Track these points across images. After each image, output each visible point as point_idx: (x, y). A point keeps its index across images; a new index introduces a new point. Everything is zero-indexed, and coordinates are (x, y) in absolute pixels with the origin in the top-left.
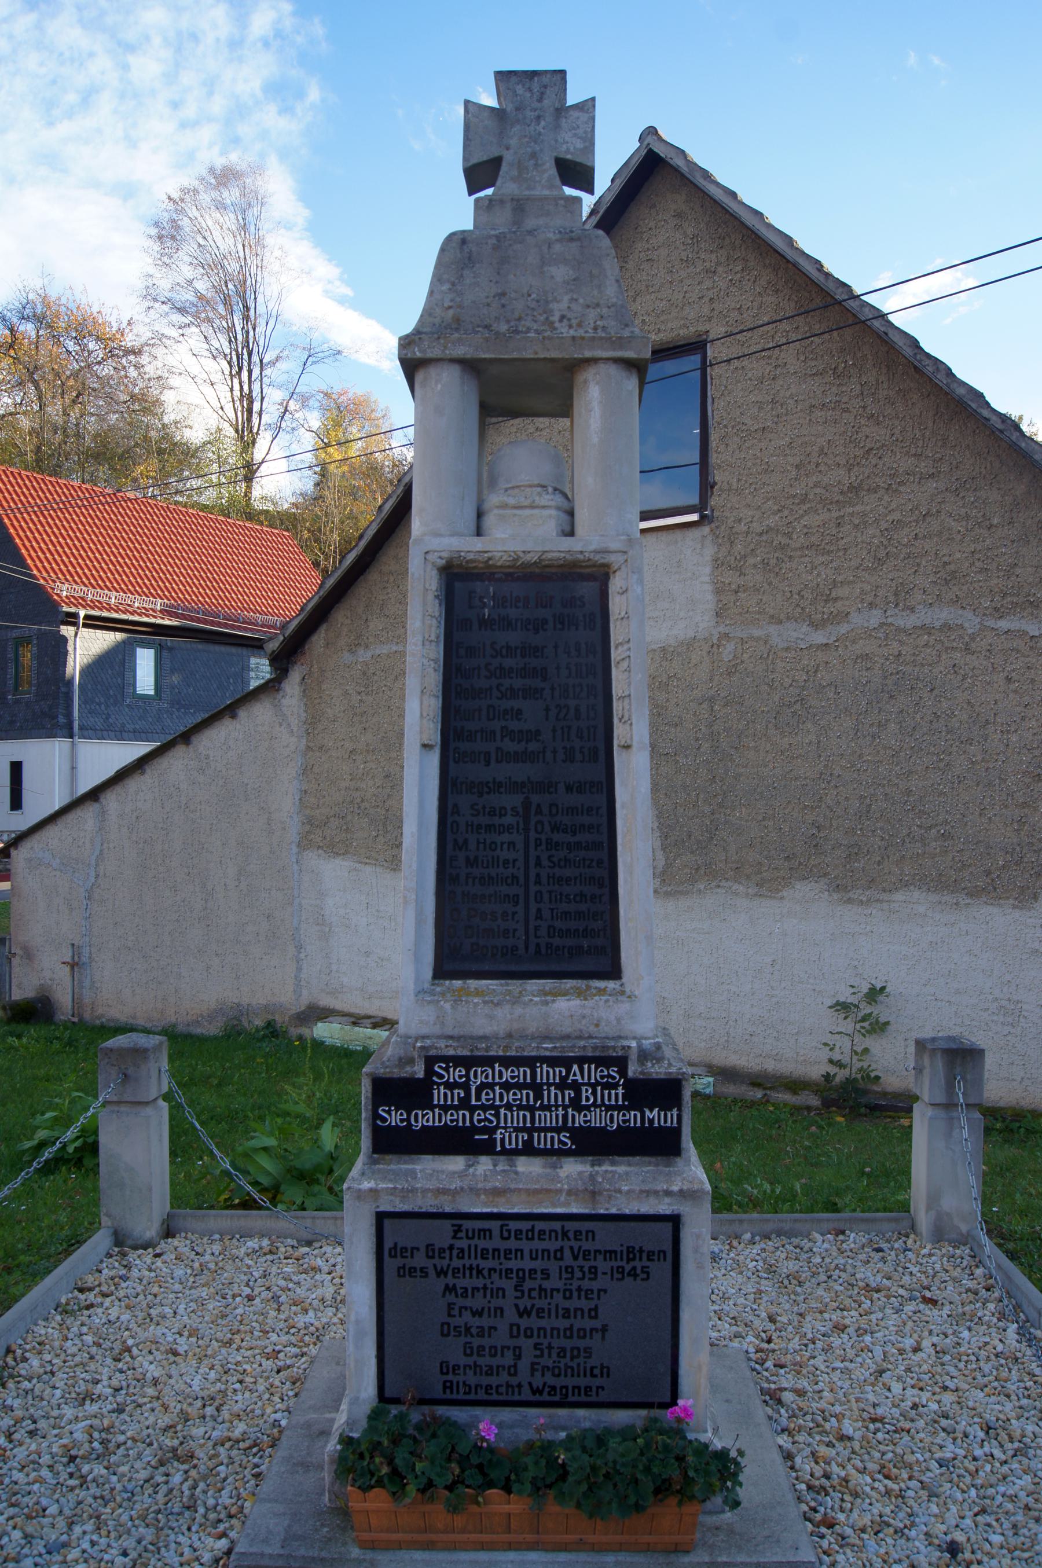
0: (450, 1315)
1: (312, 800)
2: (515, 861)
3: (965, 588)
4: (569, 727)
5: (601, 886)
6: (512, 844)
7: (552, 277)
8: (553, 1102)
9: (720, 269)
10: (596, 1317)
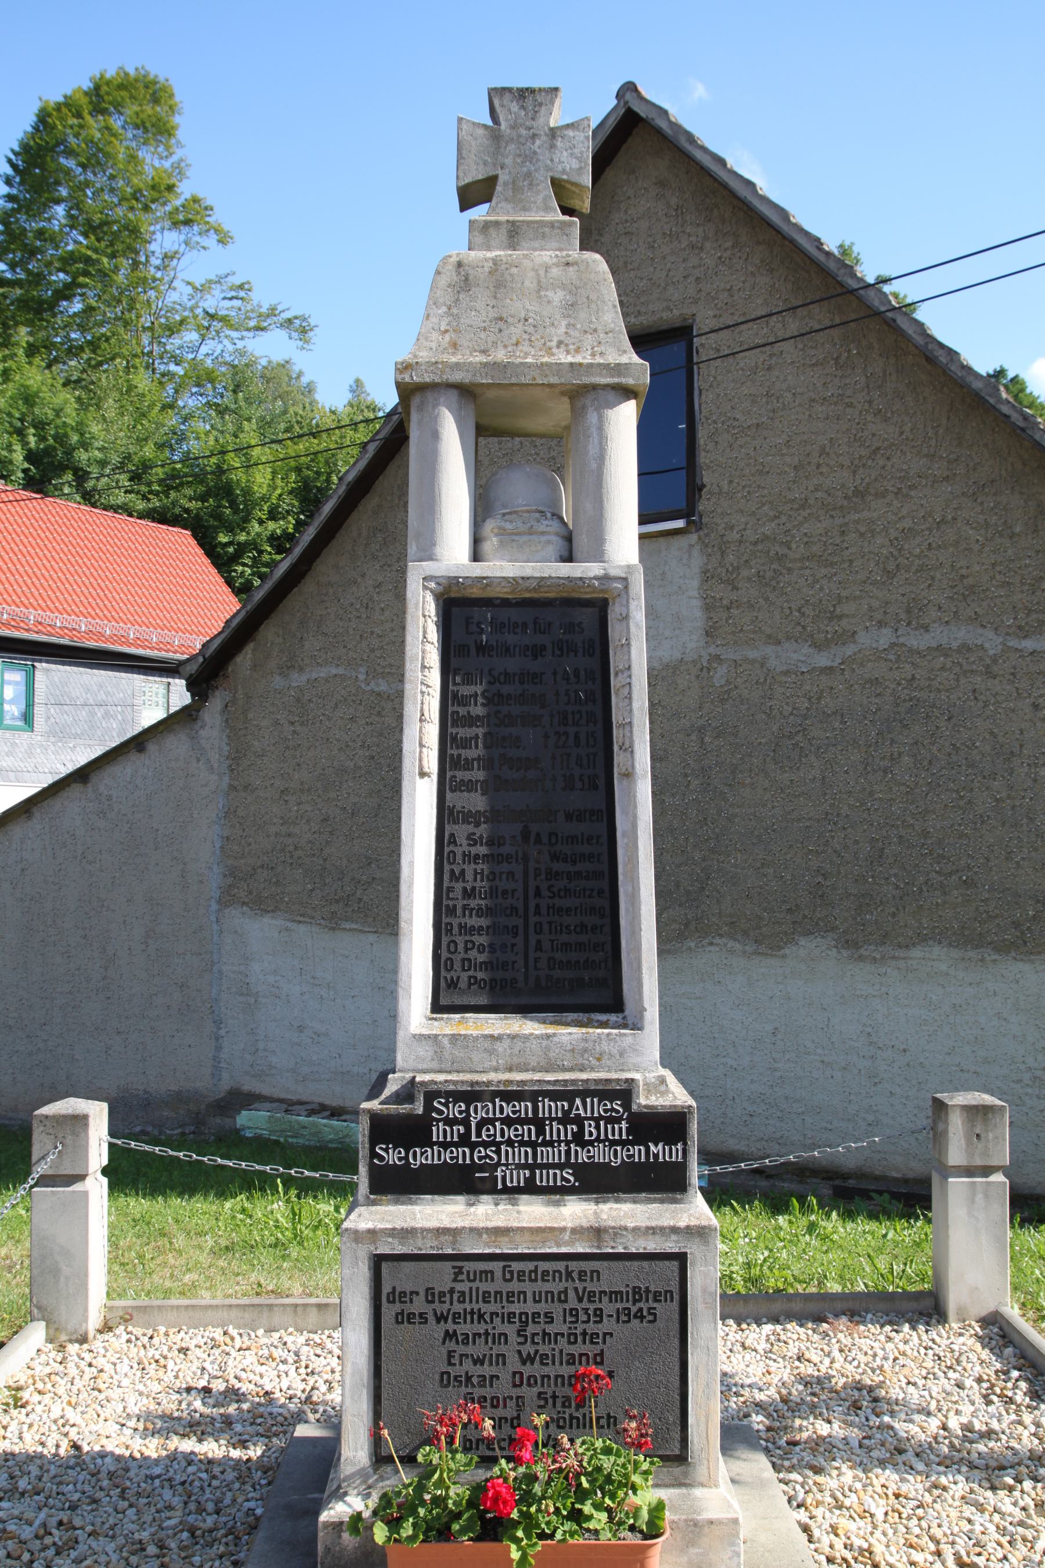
0: (450, 1364)
1: (235, 848)
2: (514, 891)
3: (985, 604)
4: (569, 755)
5: (603, 916)
6: (511, 874)
7: (549, 302)
8: (555, 1138)
9: (708, 245)
10: (602, 1363)
